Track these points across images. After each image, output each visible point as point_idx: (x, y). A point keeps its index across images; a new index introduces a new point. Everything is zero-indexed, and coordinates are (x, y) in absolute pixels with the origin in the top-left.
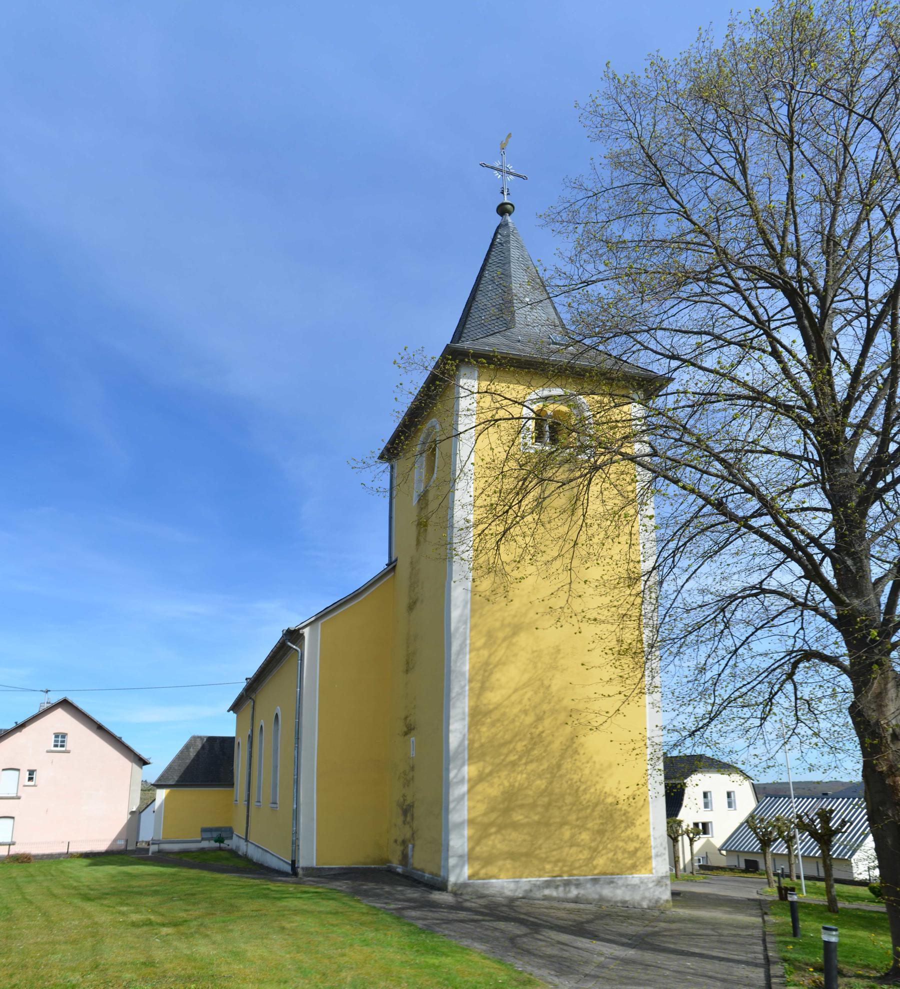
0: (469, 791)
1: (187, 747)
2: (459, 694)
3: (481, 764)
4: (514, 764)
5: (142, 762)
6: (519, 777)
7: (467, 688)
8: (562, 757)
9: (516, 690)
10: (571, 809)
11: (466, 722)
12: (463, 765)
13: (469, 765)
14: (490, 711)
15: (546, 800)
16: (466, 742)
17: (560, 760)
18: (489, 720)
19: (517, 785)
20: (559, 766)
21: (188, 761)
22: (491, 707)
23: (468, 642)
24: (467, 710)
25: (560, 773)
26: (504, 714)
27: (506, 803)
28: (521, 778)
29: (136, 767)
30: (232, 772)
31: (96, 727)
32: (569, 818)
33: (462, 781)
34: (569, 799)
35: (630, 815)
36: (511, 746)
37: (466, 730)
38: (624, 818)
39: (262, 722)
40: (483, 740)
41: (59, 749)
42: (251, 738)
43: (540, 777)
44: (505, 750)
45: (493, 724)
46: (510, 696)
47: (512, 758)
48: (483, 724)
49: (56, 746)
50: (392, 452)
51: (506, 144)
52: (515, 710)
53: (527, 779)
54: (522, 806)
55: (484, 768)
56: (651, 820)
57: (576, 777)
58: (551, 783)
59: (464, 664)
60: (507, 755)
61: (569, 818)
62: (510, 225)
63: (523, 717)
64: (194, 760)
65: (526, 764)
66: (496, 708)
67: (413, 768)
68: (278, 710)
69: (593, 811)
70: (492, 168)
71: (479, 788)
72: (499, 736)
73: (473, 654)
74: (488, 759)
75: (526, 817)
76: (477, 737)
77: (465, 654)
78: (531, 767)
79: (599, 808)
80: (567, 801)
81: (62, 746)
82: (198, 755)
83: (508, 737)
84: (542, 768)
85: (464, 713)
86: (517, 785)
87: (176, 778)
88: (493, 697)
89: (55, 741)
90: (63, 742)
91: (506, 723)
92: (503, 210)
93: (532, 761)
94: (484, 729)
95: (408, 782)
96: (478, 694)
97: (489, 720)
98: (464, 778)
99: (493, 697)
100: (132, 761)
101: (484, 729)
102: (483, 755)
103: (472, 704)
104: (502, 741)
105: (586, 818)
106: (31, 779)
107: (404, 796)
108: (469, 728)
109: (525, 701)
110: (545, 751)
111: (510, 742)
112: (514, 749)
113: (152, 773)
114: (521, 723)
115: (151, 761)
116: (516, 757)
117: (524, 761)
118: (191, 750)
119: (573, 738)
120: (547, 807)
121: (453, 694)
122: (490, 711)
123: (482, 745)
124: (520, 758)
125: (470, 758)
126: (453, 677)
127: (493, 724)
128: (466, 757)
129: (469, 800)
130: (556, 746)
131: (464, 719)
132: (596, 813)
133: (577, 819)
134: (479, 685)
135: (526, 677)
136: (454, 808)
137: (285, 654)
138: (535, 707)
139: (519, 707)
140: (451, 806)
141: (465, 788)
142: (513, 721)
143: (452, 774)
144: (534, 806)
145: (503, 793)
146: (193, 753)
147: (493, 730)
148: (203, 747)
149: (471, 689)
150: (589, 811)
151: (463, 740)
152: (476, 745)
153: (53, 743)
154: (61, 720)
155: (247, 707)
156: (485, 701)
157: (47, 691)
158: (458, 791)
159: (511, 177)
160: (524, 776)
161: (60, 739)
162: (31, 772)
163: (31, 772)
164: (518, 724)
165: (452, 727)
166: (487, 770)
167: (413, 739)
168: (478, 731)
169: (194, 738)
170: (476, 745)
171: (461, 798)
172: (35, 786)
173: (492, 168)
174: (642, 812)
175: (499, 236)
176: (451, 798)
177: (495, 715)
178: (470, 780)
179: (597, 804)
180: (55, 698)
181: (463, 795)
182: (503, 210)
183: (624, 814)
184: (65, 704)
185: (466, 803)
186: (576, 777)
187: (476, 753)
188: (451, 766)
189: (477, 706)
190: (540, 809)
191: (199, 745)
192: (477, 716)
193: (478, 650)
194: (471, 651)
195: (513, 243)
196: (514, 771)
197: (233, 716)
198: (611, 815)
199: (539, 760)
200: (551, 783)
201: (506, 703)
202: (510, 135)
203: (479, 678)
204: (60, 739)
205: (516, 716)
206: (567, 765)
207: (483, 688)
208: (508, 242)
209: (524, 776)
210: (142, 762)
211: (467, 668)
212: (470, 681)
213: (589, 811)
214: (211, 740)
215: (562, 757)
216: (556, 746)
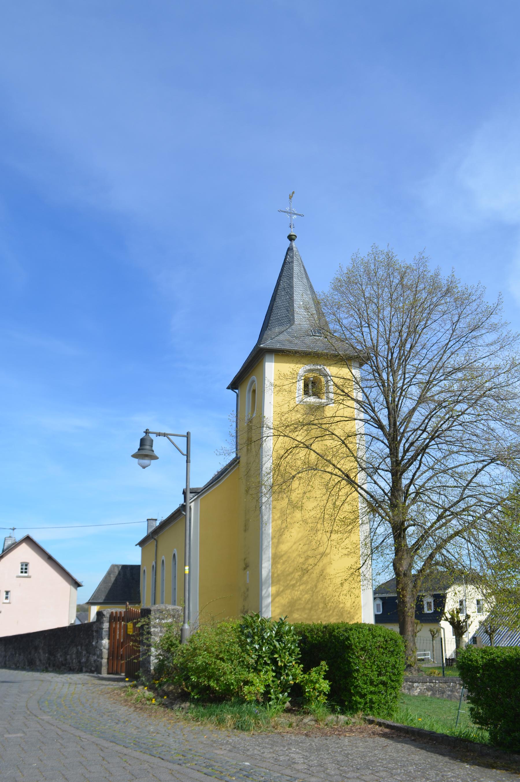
0: (272, 601)
1: (109, 573)
2: (267, 546)
3: (278, 586)
4: (294, 586)
5: (77, 585)
6: (296, 593)
7: (271, 543)
8: (318, 581)
9: (295, 543)
10: (322, 611)
11: (270, 563)
12: (269, 587)
13: (272, 586)
14: (282, 556)
15: (310, 606)
16: (270, 574)
17: (316, 583)
18: (281, 561)
19: (295, 598)
20: (316, 586)
21: (110, 585)
22: (283, 553)
23: (271, 516)
24: (271, 555)
25: (317, 590)
26: (289, 557)
27: (290, 608)
28: (297, 593)
29: (73, 589)
30: (139, 593)
31: (47, 558)
32: (321, 616)
33: (268, 596)
34: (321, 606)
35: (352, 613)
36: (293, 576)
37: (270, 567)
38: (349, 616)
39: (163, 557)
40: (279, 572)
41: (24, 574)
42: (155, 569)
43: (307, 593)
44: (290, 578)
45: (284, 563)
46: (292, 547)
47: (293, 582)
48: (278, 563)
49: (22, 572)
50: (234, 385)
51: (292, 197)
52: (295, 555)
53: (301, 594)
54: (298, 610)
55: (279, 588)
56: (362, 617)
57: (325, 593)
58: (312, 596)
59: (269, 530)
60: (291, 580)
61: (321, 616)
62: (294, 249)
63: (298, 558)
64: (114, 584)
65: (300, 585)
66: (284, 554)
67: (248, 590)
68: (175, 551)
69: (333, 612)
70: (285, 212)
71: (277, 599)
72: (287, 569)
73: (274, 522)
74: (281, 583)
75: (300, 616)
76: (276, 571)
77: (270, 523)
78: (301, 588)
79: (336, 610)
80: (320, 607)
81: (26, 572)
82: (116, 580)
83: (291, 570)
84: (307, 588)
85: (269, 557)
86: (295, 598)
87: (103, 598)
88: (284, 547)
89: (22, 569)
90: (26, 569)
91: (290, 562)
92: (291, 238)
93: (302, 584)
94: (279, 566)
95: (245, 598)
96: (276, 546)
97: (281, 561)
98: (269, 594)
99: (284, 547)
100: (70, 584)
101: (279, 566)
102: (279, 580)
103: (274, 552)
104: (288, 573)
105: (329, 616)
106: (7, 598)
107: (244, 606)
108: (272, 566)
109: (299, 549)
110: (309, 578)
111: (292, 573)
112: (294, 577)
113: (86, 593)
114: (298, 562)
115: (83, 584)
116: (295, 582)
117: (298, 584)
118: (112, 575)
119: (322, 571)
120: (311, 609)
121: (264, 547)
122: (282, 556)
123: (278, 575)
124: (297, 583)
125: (272, 583)
126: (264, 537)
127: (284, 563)
128: (270, 582)
129: (272, 606)
130: (314, 576)
131: (269, 561)
132: (335, 613)
133: (325, 617)
134: (276, 541)
135: (300, 535)
136: (265, 611)
137: (179, 515)
138: (305, 552)
139: (297, 553)
140: (264, 610)
141: (270, 600)
142: (293, 561)
143: (264, 592)
144: (304, 609)
145: (288, 602)
146: (113, 579)
147: (284, 566)
148: (119, 573)
149: (273, 543)
150: (331, 612)
151: (269, 572)
152: (275, 575)
153: (20, 570)
154: (24, 552)
155: (152, 544)
156: (280, 550)
157: (14, 529)
158: (267, 601)
159: (295, 216)
160: (299, 592)
161: (25, 568)
162: (7, 593)
163: (7, 593)
164: (296, 563)
165: (263, 565)
166: (281, 589)
167: (248, 572)
168: (276, 567)
169: (113, 566)
170: (275, 575)
171: (268, 606)
172: (9, 603)
173: (285, 212)
174: (358, 612)
175: (288, 257)
176: (263, 606)
177: (284, 558)
178: (272, 595)
179: (335, 608)
180: (19, 536)
181: (269, 604)
182: (291, 238)
183: (349, 613)
184: (28, 540)
185: (270, 608)
186: (325, 593)
187: (275, 579)
188: (263, 588)
189: (275, 553)
190: (307, 611)
191: (117, 572)
192: (276, 558)
193: (276, 520)
194: (273, 521)
195: (295, 263)
196: (293, 590)
197: (139, 549)
198: (342, 614)
199: (306, 583)
200: (312, 596)
201: (290, 551)
202: (293, 193)
203: (277, 536)
204: (25, 568)
205: (295, 558)
206: (320, 586)
207: (279, 543)
208: (292, 262)
209: (299, 592)
210: (77, 585)
211: (271, 531)
212: (272, 539)
213: (331, 612)
214: (124, 567)
215: (318, 581)
216: (314, 576)
